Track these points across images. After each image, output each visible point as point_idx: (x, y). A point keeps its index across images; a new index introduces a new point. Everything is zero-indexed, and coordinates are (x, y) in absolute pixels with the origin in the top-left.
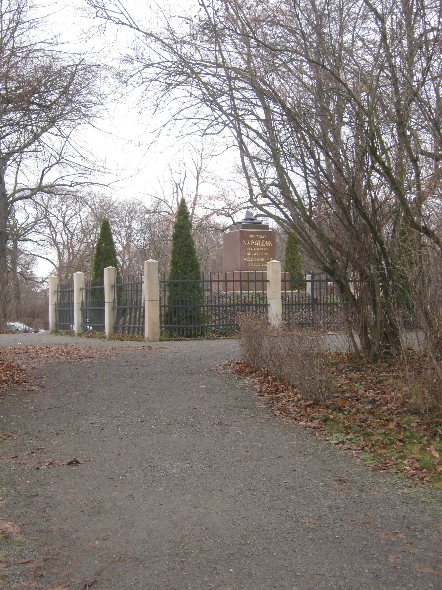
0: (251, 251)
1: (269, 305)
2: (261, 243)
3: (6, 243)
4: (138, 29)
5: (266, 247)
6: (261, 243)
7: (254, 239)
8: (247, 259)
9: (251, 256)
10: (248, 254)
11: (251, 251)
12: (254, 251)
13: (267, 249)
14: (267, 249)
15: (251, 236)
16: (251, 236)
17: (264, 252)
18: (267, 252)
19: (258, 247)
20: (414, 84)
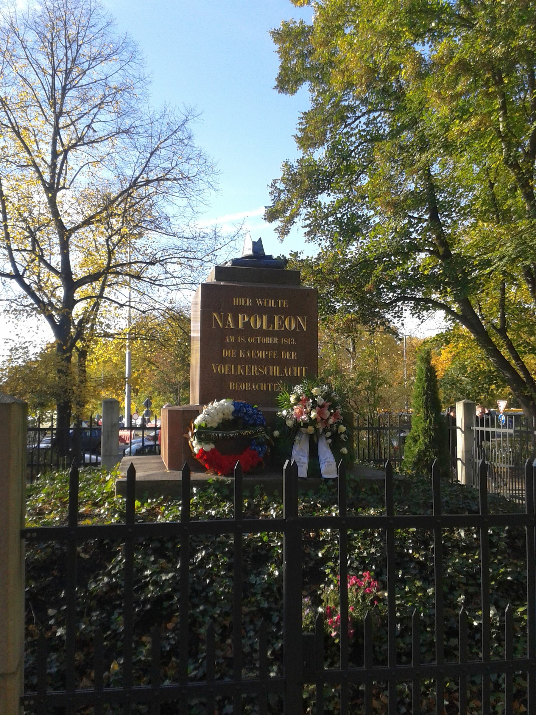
0: (236, 346)
1: (286, 24)
2: (271, 321)
3: (47, 612)
4: (101, 121)
5: (287, 334)
6: (271, 321)
7: (250, 311)
8: (224, 370)
9: (237, 361)
10: (229, 353)
11: (236, 346)
12: (248, 347)
13: (291, 341)
14: (291, 341)
15: (236, 301)
16: (236, 301)
17: (279, 348)
18: (289, 348)
19: (261, 333)
20: (337, 641)
